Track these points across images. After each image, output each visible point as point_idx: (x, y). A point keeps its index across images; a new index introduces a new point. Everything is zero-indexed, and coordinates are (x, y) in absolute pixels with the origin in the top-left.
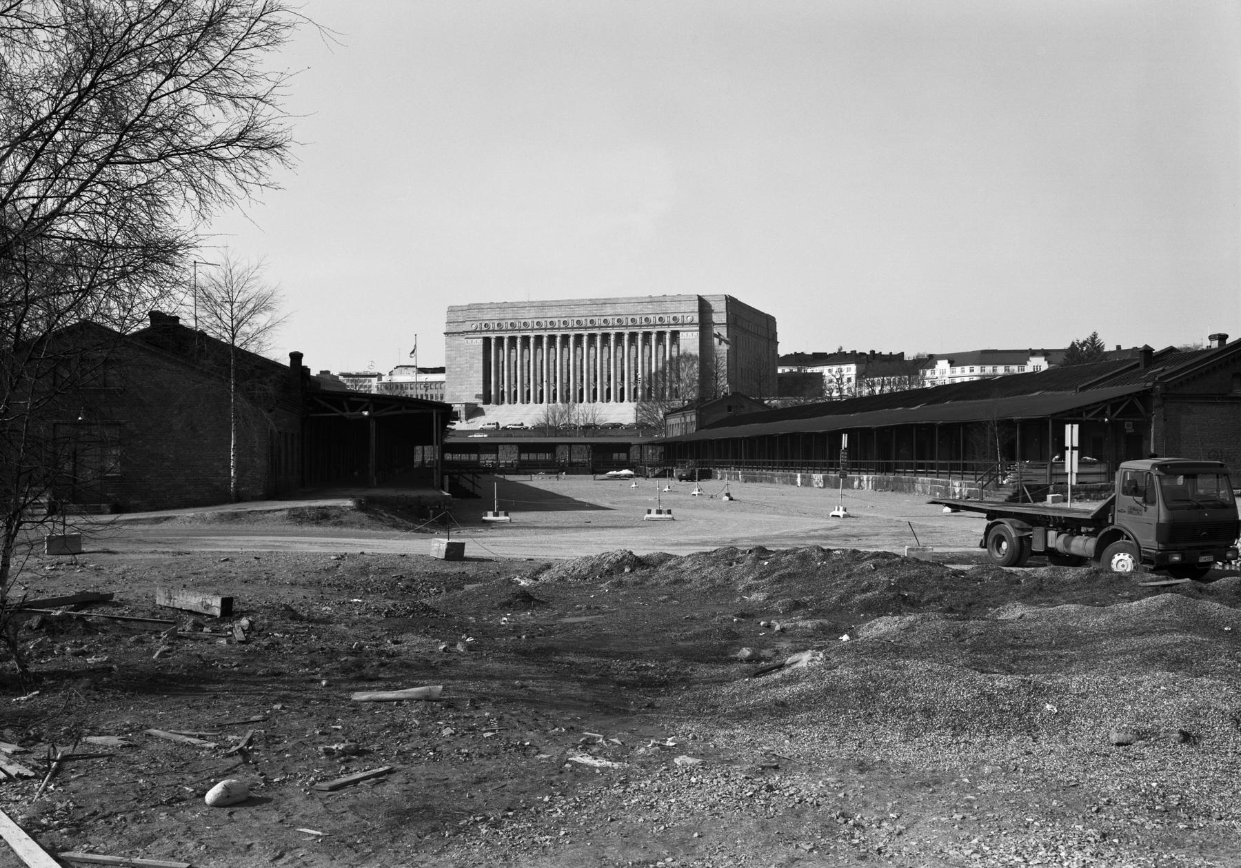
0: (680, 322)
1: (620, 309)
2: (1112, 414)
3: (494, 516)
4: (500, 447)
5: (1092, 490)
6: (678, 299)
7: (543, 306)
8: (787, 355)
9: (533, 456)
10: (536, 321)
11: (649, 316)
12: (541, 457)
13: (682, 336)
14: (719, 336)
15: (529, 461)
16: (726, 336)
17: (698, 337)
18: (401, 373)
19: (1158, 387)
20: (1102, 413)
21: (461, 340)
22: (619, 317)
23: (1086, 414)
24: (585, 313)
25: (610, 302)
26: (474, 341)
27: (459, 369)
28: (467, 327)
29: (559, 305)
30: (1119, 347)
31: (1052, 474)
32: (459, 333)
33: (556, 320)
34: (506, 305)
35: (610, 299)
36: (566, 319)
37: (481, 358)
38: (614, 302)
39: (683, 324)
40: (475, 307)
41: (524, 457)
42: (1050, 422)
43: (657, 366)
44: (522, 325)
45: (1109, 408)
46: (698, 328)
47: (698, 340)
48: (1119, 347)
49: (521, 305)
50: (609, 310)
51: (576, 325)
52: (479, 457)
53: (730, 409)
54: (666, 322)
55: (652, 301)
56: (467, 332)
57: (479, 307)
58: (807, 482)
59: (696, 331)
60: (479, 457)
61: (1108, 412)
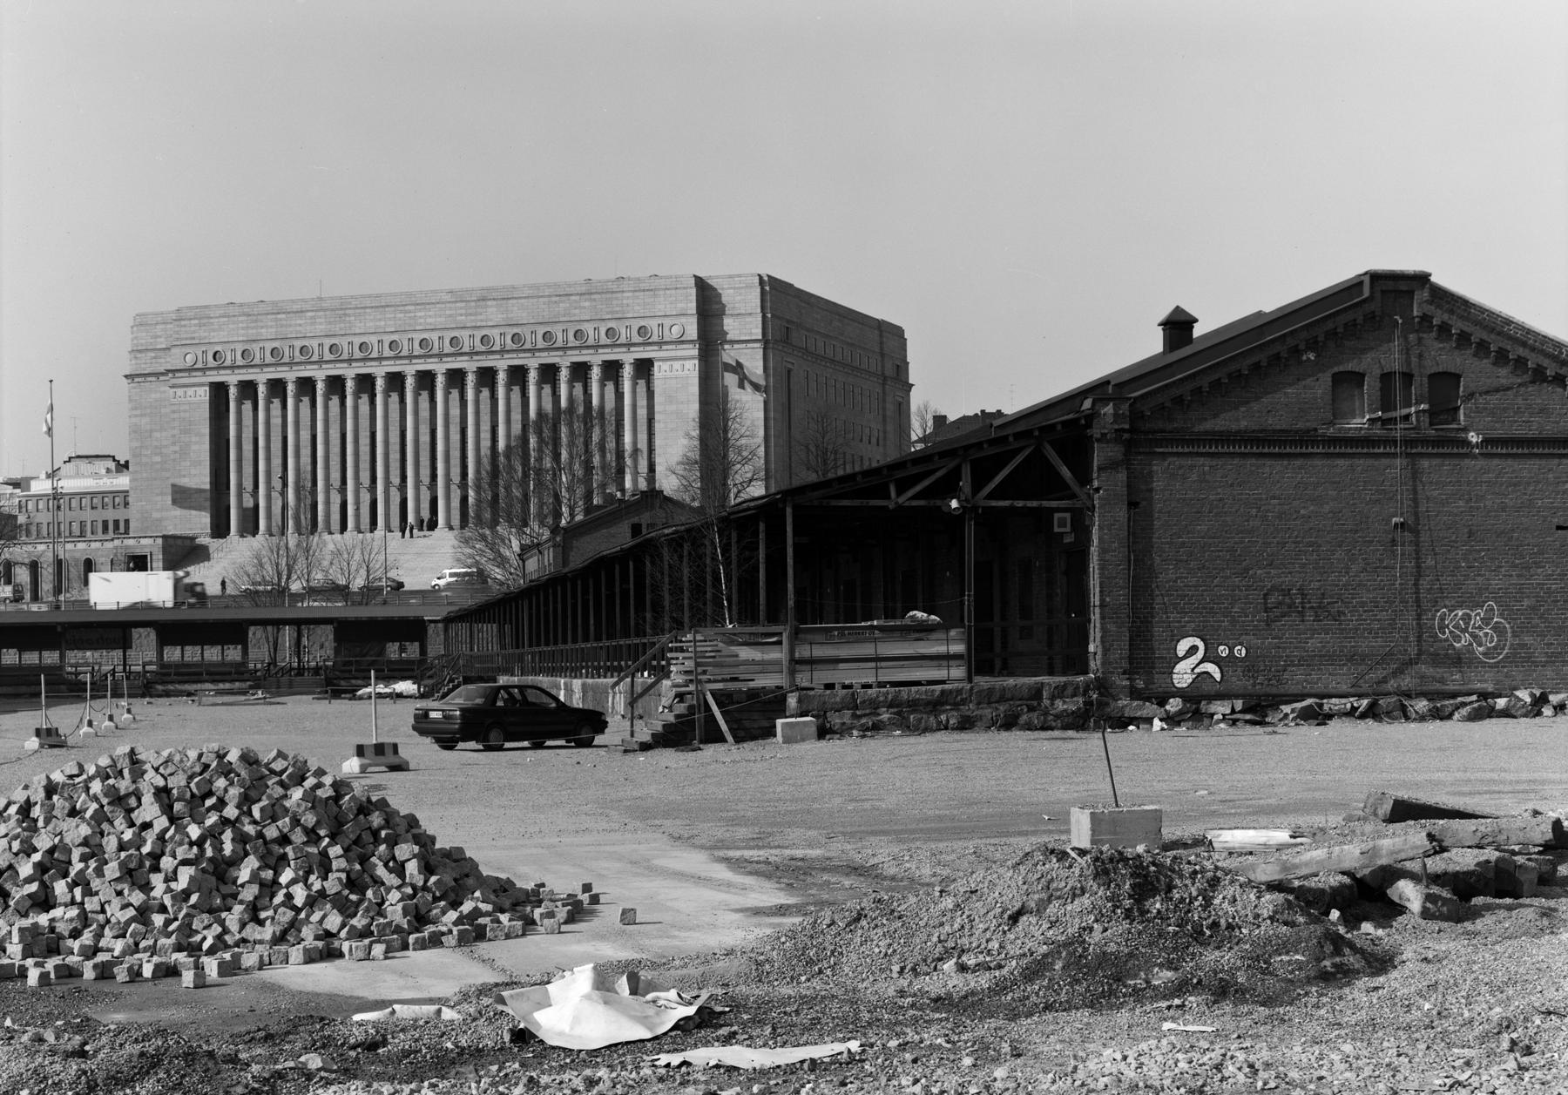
0: (655, 338)
4: (135, 632)
5: (913, 705)
6: (650, 287)
7: (342, 309)
8: (965, 418)
9: (192, 654)
10: (328, 342)
11: (584, 327)
12: (212, 654)
14: (738, 368)
16: (760, 371)
17: (696, 373)
19: (1109, 409)
20: (948, 487)
21: (160, 391)
22: (516, 330)
23: (899, 494)
24: (440, 321)
25: (495, 295)
26: (190, 391)
27: (158, 459)
28: (175, 360)
29: (382, 305)
30: (1178, 326)
31: (796, 663)
32: (157, 375)
34: (262, 308)
35: (496, 290)
36: (395, 337)
38: (505, 296)
39: (660, 344)
40: (190, 314)
41: (173, 654)
42: (789, 511)
43: (508, 435)
44: (297, 353)
45: (966, 472)
46: (695, 352)
47: (696, 381)
48: (1178, 326)
49: (296, 307)
51: (417, 351)
52: (62, 657)
54: (623, 340)
55: (590, 291)
56: (174, 371)
57: (202, 315)
59: (692, 358)
60: (62, 657)
61: (965, 484)
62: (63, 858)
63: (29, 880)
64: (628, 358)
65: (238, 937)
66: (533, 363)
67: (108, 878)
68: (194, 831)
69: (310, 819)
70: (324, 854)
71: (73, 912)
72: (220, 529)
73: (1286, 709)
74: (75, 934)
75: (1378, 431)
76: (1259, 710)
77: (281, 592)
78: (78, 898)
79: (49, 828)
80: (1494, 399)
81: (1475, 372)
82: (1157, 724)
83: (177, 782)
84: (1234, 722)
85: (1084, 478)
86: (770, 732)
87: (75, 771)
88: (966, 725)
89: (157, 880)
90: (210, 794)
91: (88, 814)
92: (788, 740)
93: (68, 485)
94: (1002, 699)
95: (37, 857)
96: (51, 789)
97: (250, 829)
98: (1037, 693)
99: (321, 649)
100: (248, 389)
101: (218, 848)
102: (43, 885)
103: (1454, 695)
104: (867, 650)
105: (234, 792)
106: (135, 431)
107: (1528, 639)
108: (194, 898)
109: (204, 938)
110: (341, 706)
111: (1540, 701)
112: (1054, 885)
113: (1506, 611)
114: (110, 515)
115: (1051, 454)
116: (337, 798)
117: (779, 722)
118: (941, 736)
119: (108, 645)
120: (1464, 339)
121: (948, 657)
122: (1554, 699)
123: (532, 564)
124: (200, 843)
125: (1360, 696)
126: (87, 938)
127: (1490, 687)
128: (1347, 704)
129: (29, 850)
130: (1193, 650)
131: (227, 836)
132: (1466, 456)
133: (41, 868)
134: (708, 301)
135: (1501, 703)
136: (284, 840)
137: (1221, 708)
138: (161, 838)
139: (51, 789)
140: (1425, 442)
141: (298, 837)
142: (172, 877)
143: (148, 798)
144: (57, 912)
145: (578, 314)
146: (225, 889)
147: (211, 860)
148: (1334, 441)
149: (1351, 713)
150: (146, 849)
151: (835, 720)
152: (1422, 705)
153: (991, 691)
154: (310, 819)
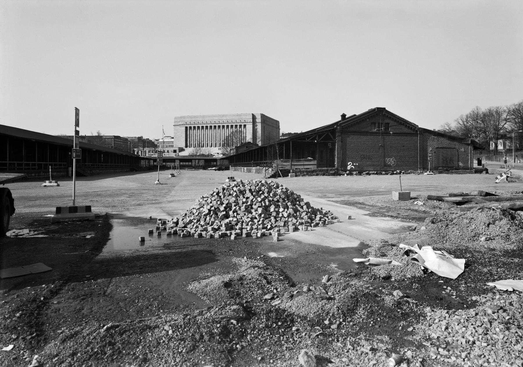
1: (228, 118)
2: (319, 139)
3: (49, 183)
5: (309, 172)
6: (246, 115)
7: (204, 117)
9: (184, 163)
12: (187, 163)
13: (247, 126)
15: (186, 165)
18: (166, 139)
19: (339, 127)
20: (314, 139)
21: (178, 127)
23: (308, 139)
24: (217, 119)
28: (180, 123)
30: (343, 116)
31: (292, 165)
33: (208, 121)
37: (185, 133)
38: (226, 116)
41: (181, 163)
48: (343, 116)
50: (224, 118)
53: (247, 147)
55: (238, 115)
57: (184, 117)
58: (249, 171)
61: (317, 138)
62: (230, 206)
63: (223, 211)
64: (243, 124)
65: (275, 225)
66: (230, 125)
67: (242, 210)
68: (259, 199)
69: (283, 196)
70: (287, 204)
71: (235, 219)
72: (186, 146)
73: (364, 173)
74: (237, 225)
75: (377, 131)
76: (360, 173)
77: (196, 155)
78: (235, 216)
79: (225, 198)
80: (394, 127)
81: (392, 123)
82: (345, 175)
83: (253, 188)
84: (356, 175)
85: (335, 138)
86: (288, 176)
87: (229, 185)
88: (317, 175)
89: (253, 211)
90: (260, 190)
91: (234, 195)
92: (291, 177)
93: (165, 140)
94: (322, 171)
95: (224, 205)
96: (224, 189)
97: (271, 199)
98: (327, 170)
99: (202, 163)
100: (190, 128)
101: (265, 203)
102: (226, 212)
103: (388, 171)
104: (302, 163)
105: (266, 190)
106: (174, 133)
107: (399, 163)
108: (263, 215)
109: (267, 226)
110: (205, 171)
111: (401, 172)
112: (494, 217)
113: (396, 159)
114: (170, 144)
115: (330, 134)
116: (287, 191)
117: (289, 174)
118: (314, 177)
119: (172, 162)
120: (390, 118)
121: (314, 164)
122: (403, 172)
123: (232, 152)
124: (261, 202)
125: (375, 171)
126: (239, 225)
127: (393, 170)
128: (373, 172)
129: (222, 204)
130: (350, 164)
131: (267, 200)
132: (390, 136)
133: (225, 208)
134: (254, 117)
135: (395, 172)
136: (278, 201)
137: (354, 173)
138: (252, 201)
139: (224, 189)
140: (384, 133)
141: (281, 200)
142: (256, 210)
143: (248, 192)
144: (231, 219)
145: (236, 118)
146: (268, 213)
147: (264, 206)
148: (371, 133)
149: (373, 174)
150: (249, 203)
151: (298, 174)
152: (384, 173)
153: (321, 170)
154: (283, 196)
